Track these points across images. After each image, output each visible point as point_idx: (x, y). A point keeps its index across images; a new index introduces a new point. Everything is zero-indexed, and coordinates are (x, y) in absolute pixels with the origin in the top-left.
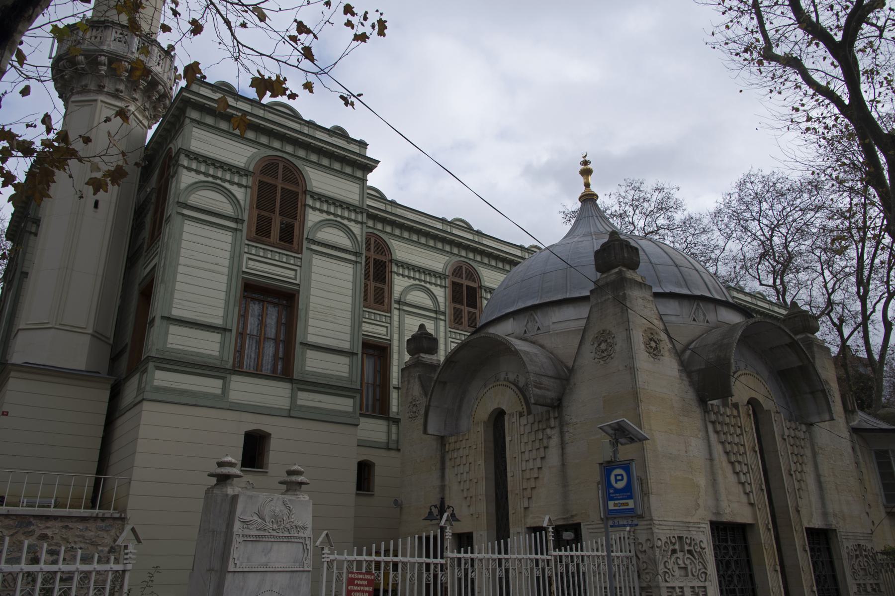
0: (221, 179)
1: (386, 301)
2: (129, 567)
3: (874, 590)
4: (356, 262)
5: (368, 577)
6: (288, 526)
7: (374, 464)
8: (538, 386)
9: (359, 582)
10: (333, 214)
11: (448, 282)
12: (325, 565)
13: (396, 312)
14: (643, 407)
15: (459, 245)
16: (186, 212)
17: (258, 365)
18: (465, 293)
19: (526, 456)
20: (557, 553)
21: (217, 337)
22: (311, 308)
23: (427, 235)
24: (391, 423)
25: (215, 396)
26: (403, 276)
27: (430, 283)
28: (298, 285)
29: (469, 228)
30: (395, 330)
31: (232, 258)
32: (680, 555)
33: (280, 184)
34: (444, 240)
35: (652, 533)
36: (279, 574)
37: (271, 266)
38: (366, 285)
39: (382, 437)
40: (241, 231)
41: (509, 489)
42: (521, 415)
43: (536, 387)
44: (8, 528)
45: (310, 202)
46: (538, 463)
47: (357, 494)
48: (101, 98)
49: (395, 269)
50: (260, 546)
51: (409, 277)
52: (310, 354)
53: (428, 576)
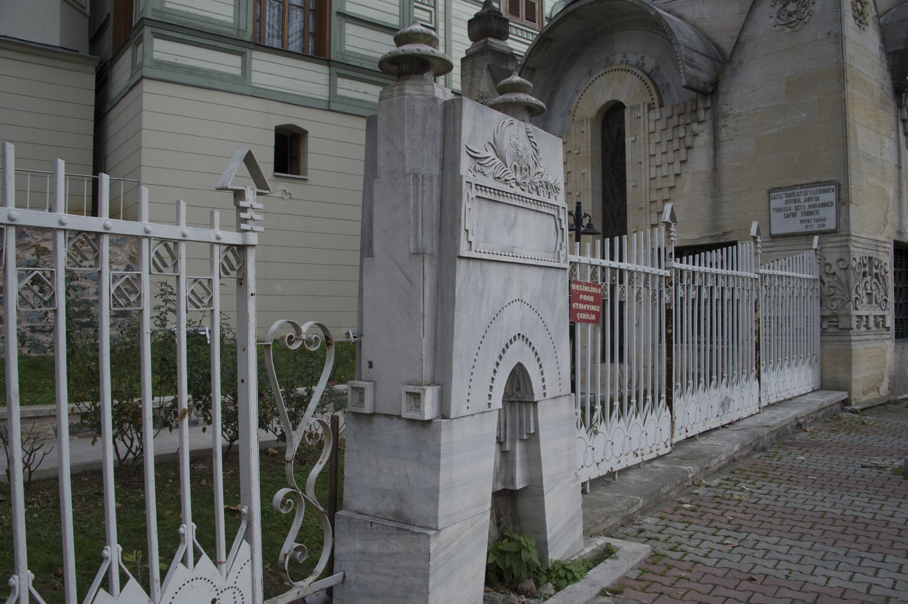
2: (253, 239)
3: (877, 325)
5: (594, 290)
6: (536, 180)
8: (691, 63)
14: (849, 88)
17: (283, 35)
19: (658, 160)
25: (234, 77)
30: (441, 17)
32: (868, 278)
35: (849, 252)
41: (629, 201)
42: (650, 107)
46: (677, 168)
52: (351, 29)
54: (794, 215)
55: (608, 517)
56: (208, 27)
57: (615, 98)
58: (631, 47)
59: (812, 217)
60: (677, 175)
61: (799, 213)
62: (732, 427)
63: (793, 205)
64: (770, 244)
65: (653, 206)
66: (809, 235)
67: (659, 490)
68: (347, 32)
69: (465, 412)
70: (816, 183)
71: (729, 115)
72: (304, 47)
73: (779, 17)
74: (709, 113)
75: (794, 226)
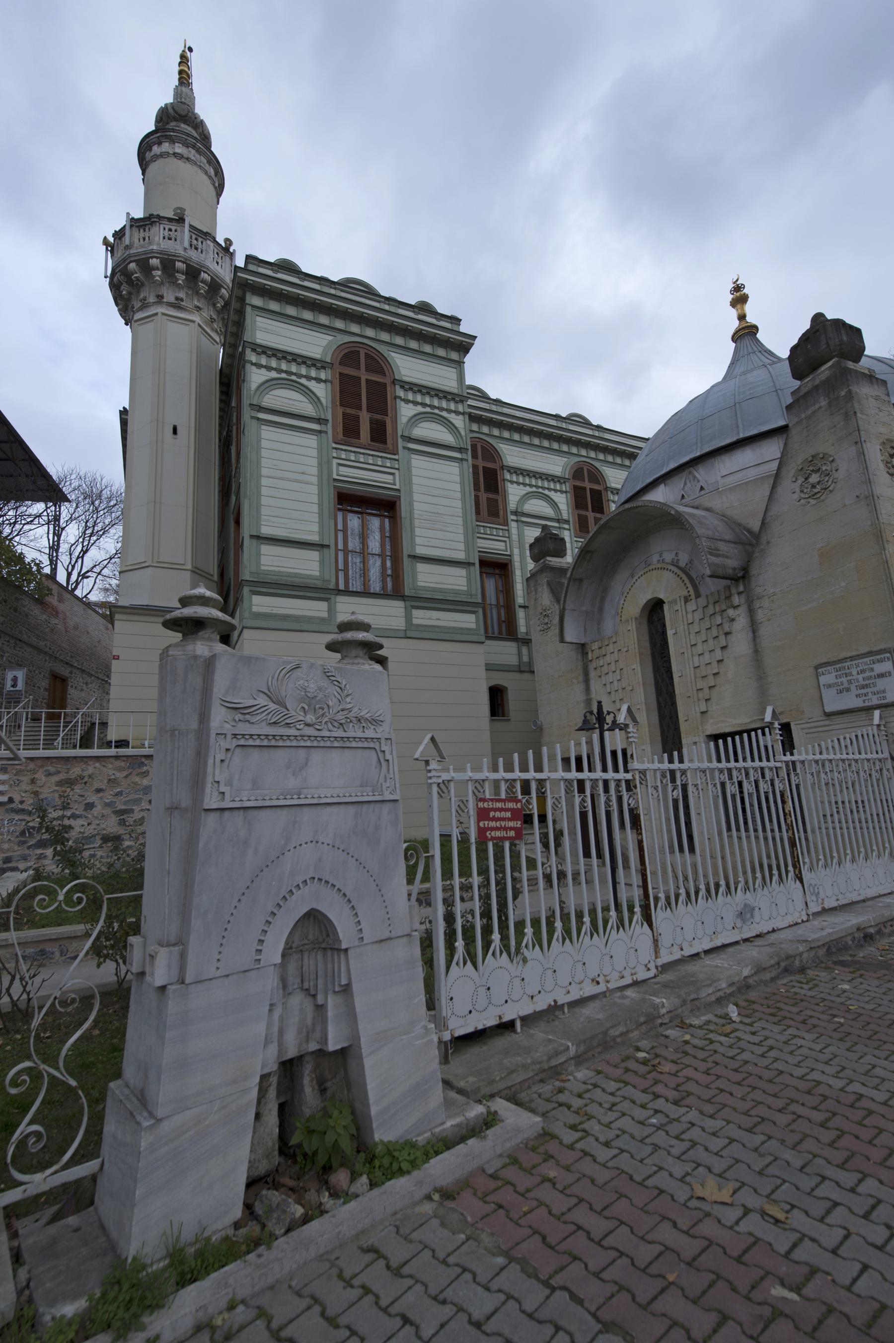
0: (295, 374)
1: (501, 512)
4: (462, 460)
5: (511, 805)
6: (340, 717)
7: (506, 688)
8: (714, 552)
9: (498, 814)
10: (429, 406)
11: (566, 487)
12: (435, 789)
13: (514, 525)
15: (578, 443)
16: (262, 416)
17: (366, 582)
18: (588, 495)
19: (700, 649)
20: (788, 758)
21: (314, 555)
22: (416, 516)
23: (541, 434)
24: (520, 644)
25: (322, 620)
26: (518, 483)
27: (549, 489)
28: (398, 490)
29: (586, 423)
30: (515, 544)
31: (320, 465)
33: (364, 376)
34: (560, 439)
36: (329, 809)
37: (364, 471)
38: (477, 498)
39: (513, 660)
40: (326, 432)
43: (711, 554)
44: (120, 770)
45: (401, 393)
46: (718, 655)
47: (492, 720)
48: (161, 309)
49: (507, 476)
50: (280, 756)
51: (525, 485)
52: (421, 567)
53: (608, 800)
54: (848, 690)
55: (512, 1072)
56: (297, 581)
57: (655, 596)
58: (664, 548)
59: (869, 690)
60: (720, 661)
61: (853, 687)
62: (760, 941)
63: (844, 680)
64: (827, 723)
65: (701, 694)
66: (869, 709)
67: (605, 1033)
68: (418, 570)
69: (212, 972)
70: (868, 653)
71: (763, 596)
72: (384, 587)
73: (802, 491)
74: (743, 596)
75: (851, 701)
